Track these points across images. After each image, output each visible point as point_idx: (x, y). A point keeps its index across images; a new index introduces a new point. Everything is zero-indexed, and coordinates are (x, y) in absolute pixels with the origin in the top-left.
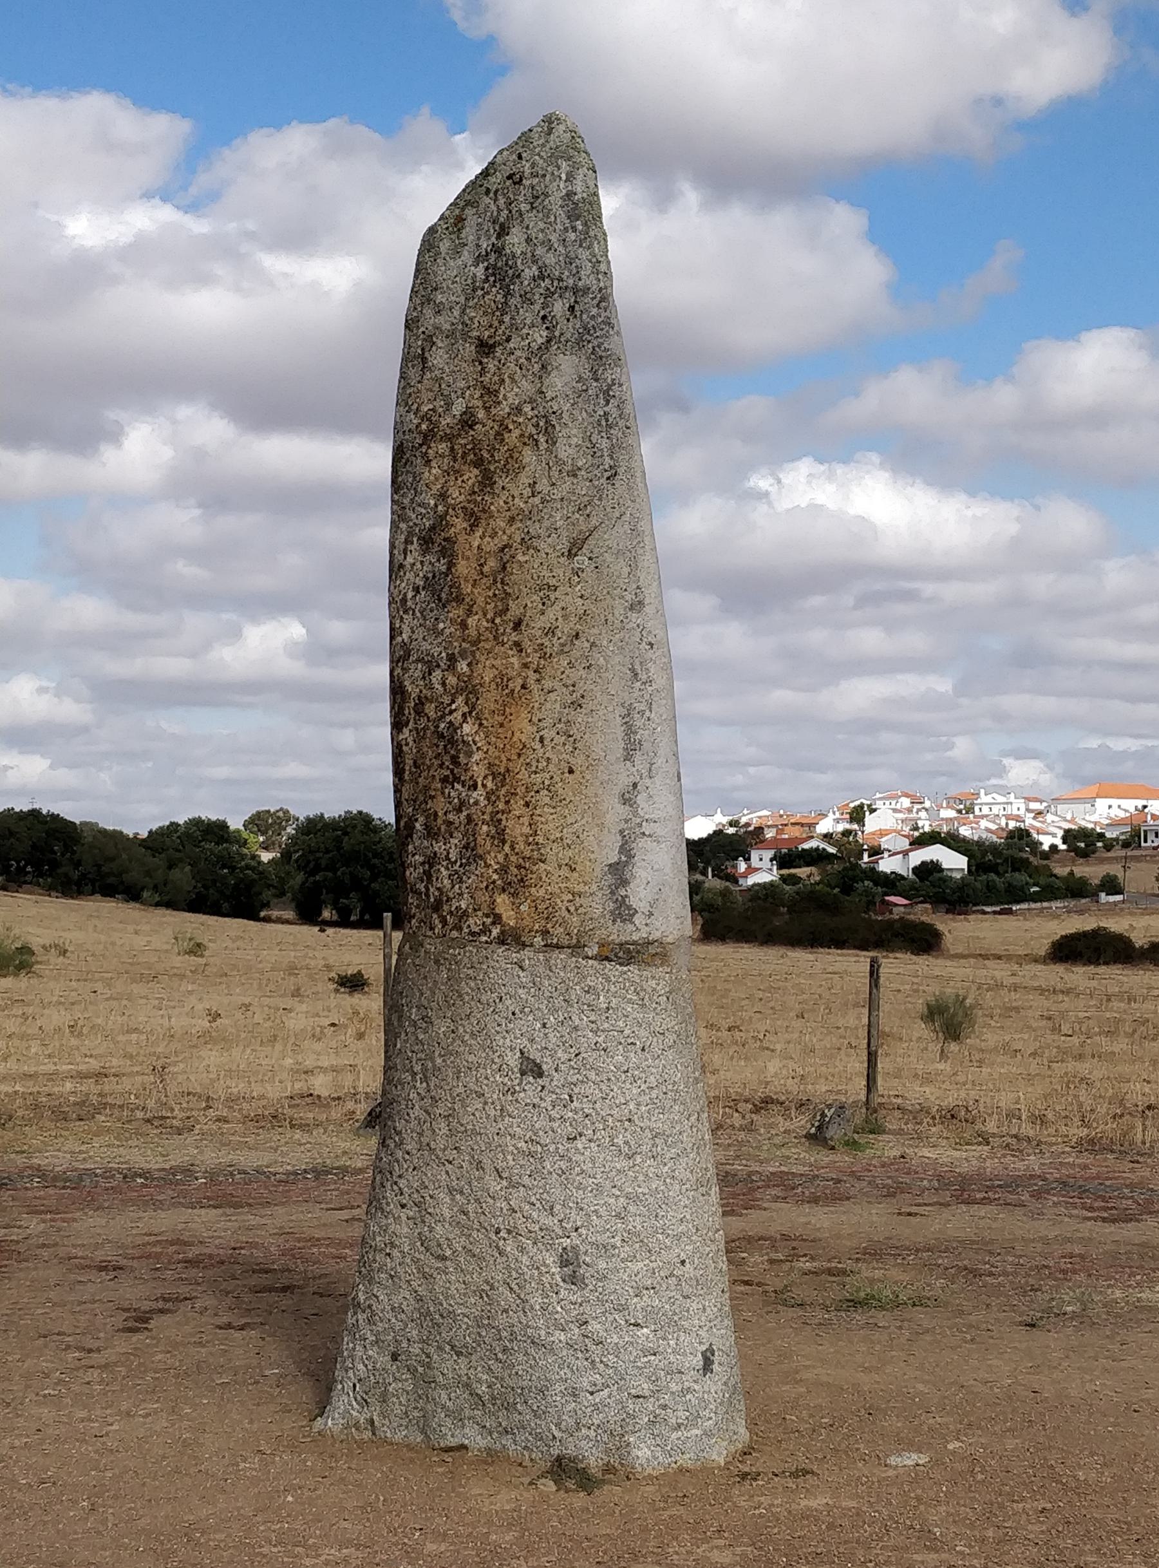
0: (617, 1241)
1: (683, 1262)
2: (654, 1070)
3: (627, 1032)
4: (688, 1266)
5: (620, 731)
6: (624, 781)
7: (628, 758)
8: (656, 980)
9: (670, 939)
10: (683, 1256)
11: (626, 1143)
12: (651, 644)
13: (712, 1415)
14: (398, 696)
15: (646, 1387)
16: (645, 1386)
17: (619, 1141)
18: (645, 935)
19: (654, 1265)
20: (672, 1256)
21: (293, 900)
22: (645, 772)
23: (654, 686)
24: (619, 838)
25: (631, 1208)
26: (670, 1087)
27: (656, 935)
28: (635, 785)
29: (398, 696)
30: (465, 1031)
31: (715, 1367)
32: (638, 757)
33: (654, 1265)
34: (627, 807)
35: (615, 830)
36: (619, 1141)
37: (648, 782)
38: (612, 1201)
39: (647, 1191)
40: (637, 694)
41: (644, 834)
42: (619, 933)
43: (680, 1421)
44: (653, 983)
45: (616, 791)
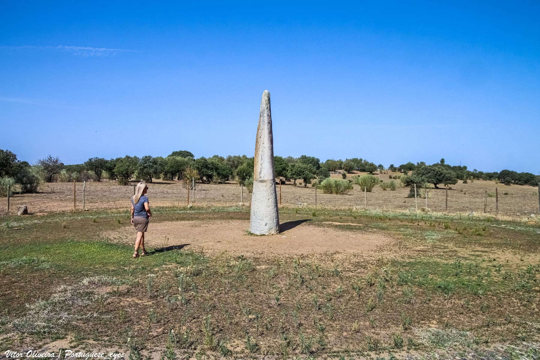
8: (264, 184)
42: (260, 179)
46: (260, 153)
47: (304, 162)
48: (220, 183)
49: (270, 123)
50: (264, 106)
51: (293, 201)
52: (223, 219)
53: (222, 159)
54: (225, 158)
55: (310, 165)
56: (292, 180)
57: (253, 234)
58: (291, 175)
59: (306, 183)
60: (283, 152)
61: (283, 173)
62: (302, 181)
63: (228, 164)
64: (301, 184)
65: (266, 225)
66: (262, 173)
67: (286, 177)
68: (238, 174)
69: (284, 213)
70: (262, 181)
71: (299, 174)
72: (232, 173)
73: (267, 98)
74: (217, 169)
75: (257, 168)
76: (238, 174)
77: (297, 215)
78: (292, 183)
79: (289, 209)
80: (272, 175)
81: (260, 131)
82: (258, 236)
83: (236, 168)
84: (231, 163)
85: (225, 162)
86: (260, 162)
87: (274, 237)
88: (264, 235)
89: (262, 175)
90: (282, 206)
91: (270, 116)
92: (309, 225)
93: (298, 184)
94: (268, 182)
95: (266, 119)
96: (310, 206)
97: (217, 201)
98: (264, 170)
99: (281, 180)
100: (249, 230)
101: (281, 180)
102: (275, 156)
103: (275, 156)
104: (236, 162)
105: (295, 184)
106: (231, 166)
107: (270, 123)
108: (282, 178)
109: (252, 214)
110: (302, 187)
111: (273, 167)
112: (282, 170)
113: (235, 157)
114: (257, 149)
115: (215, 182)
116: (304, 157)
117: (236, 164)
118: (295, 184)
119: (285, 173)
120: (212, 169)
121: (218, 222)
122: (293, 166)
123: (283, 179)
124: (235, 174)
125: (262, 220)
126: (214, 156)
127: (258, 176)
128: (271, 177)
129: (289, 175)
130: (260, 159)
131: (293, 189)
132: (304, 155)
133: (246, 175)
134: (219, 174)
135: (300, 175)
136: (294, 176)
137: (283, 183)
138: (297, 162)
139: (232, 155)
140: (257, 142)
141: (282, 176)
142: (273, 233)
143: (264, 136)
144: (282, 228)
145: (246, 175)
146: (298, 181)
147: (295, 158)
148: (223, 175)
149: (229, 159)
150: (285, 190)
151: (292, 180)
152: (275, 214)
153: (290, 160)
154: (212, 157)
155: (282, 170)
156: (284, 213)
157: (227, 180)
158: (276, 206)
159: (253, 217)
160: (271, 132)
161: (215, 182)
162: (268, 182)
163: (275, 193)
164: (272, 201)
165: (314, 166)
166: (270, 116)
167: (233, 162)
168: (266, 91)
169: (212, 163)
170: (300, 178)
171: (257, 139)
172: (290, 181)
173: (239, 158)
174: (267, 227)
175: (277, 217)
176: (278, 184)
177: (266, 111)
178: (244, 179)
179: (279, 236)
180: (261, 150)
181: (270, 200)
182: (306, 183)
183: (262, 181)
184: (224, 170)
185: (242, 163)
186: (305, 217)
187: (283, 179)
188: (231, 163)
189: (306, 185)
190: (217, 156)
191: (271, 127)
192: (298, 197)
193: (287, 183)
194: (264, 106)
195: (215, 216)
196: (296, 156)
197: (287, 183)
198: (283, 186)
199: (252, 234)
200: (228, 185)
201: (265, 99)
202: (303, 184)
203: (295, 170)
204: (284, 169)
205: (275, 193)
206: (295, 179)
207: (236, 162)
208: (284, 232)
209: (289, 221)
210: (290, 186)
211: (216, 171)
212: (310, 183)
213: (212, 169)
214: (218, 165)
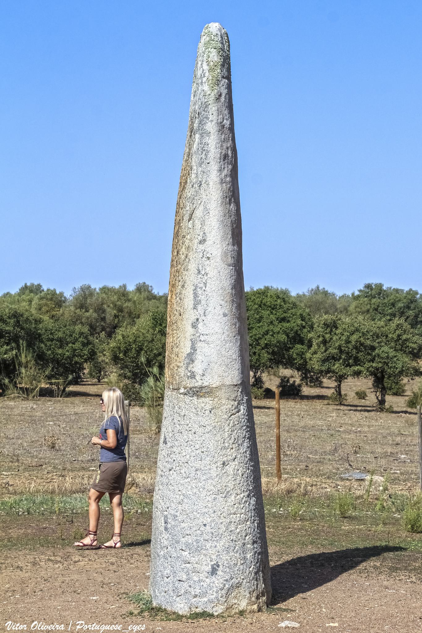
0: (178, 514)
1: (205, 525)
2: (199, 442)
3: (190, 425)
4: (207, 527)
5: (192, 297)
6: (193, 318)
7: (195, 308)
8: (206, 402)
9: (214, 386)
10: (205, 522)
11: (185, 472)
12: (208, 258)
13: (214, 593)
14: (394, 521)
15: (184, 577)
16: (184, 577)
17: (182, 471)
18: (200, 384)
19: (192, 525)
20: (200, 522)
21: (304, 295)
22: (202, 313)
23: (209, 276)
24: (190, 342)
25: (185, 500)
26: (206, 449)
27: (206, 384)
28: (197, 320)
29: (394, 521)
30: (18, 627)
31: (220, 573)
32: (199, 307)
33: (192, 525)
34: (194, 329)
35: (189, 338)
36: (182, 471)
37: (204, 318)
38: (178, 497)
39: (191, 493)
40: (200, 280)
41: (201, 340)
42: (191, 383)
43: (196, 593)
44: (203, 405)
45: (190, 322)
46: (190, 278)
47: (376, 311)
48: (45, 393)
49: (231, 160)
50: (205, 88)
51: (327, 468)
52: (47, 543)
53: (57, 300)
54: (69, 294)
55: (397, 321)
56: (326, 381)
57: (159, 609)
58: (324, 361)
59: (384, 391)
60: (291, 268)
61: (293, 352)
62: (365, 383)
63: (76, 320)
64: (361, 395)
65: (214, 571)
66: (199, 357)
67: (303, 368)
68: (115, 359)
69: (295, 517)
70: (198, 392)
71: (354, 355)
72: (92, 356)
73: (214, 56)
74: (33, 338)
75: (179, 342)
76: (115, 359)
77: (346, 527)
78: (328, 393)
79: (314, 502)
80: (237, 365)
81: (189, 192)
82: (179, 617)
83: (109, 335)
84: (91, 314)
85: (68, 312)
86: (190, 316)
87: (246, 622)
88: (205, 615)
89: (198, 367)
90: (283, 486)
91: (231, 129)
92: (394, 569)
93: (351, 398)
94: (222, 394)
95: (213, 143)
96: (398, 489)
97: (28, 468)
98: (205, 344)
99: (284, 382)
100: (147, 593)
101: (284, 382)
102: (251, 285)
103: (251, 285)
104: (110, 312)
105: (339, 398)
106: (92, 328)
107: (231, 160)
108: (287, 372)
109: (158, 523)
110: (366, 409)
111: (240, 333)
112: (282, 345)
113: (105, 290)
114: (177, 265)
115: (26, 391)
116: (373, 292)
117: (109, 317)
118: (339, 398)
119: (301, 355)
120: (16, 339)
121: (23, 557)
122: (332, 326)
123: (294, 376)
124: (105, 358)
125: (198, 550)
126: (25, 289)
127: (182, 371)
128: (233, 376)
129: (315, 364)
130: (189, 302)
131: (332, 415)
132: (374, 281)
133: (149, 363)
134: (41, 359)
135: (357, 361)
136: (337, 366)
137: (289, 392)
138: (346, 310)
139: (96, 286)
140: (176, 235)
141: (290, 363)
142: (243, 604)
143: (207, 211)
144: (282, 583)
145: (149, 363)
146: (352, 386)
147: (339, 293)
148: (57, 362)
149: (85, 297)
150: (304, 422)
151: (326, 381)
152: (250, 526)
153: (320, 301)
154: (14, 290)
155: (282, 345)
156: (295, 517)
157: (76, 381)
158: (256, 491)
159: (161, 538)
160: (233, 196)
161: (26, 391)
162: (222, 394)
163: (252, 437)
164: (237, 468)
165: (413, 326)
166: (229, 131)
167: (100, 309)
168: (214, 27)
169: (16, 315)
170: (357, 374)
171: (178, 223)
172: (320, 385)
173: (123, 293)
174: (218, 581)
175: (262, 539)
176: (269, 394)
177: (213, 108)
178: (138, 375)
179: (266, 617)
180: (192, 266)
181: (230, 469)
182: (384, 391)
183: (198, 392)
184: (62, 343)
185: (133, 317)
186: (379, 534)
187: (294, 376)
188: (91, 314)
189: (382, 402)
190: (35, 289)
191: (234, 174)
192: (349, 449)
193: (306, 390)
194: (206, 88)
195: (14, 533)
196: (345, 286)
197: (306, 390)
198: (289, 406)
199: (155, 611)
200: (77, 400)
201: (207, 58)
202: (372, 399)
203: (337, 341)
204: (297, 338)
205: (252, 437)
206: (340, 378)
207: (110, 312)
208: (291, 603)
209: (311, 550)
210: (318, 404)
211: (30, 345)
212: (398, 393)
213: (16, 339)
214: (38, 321)
